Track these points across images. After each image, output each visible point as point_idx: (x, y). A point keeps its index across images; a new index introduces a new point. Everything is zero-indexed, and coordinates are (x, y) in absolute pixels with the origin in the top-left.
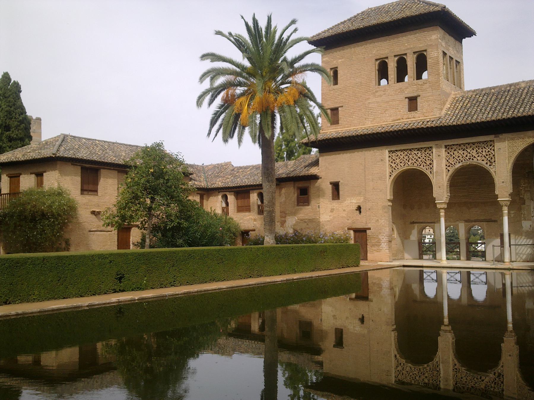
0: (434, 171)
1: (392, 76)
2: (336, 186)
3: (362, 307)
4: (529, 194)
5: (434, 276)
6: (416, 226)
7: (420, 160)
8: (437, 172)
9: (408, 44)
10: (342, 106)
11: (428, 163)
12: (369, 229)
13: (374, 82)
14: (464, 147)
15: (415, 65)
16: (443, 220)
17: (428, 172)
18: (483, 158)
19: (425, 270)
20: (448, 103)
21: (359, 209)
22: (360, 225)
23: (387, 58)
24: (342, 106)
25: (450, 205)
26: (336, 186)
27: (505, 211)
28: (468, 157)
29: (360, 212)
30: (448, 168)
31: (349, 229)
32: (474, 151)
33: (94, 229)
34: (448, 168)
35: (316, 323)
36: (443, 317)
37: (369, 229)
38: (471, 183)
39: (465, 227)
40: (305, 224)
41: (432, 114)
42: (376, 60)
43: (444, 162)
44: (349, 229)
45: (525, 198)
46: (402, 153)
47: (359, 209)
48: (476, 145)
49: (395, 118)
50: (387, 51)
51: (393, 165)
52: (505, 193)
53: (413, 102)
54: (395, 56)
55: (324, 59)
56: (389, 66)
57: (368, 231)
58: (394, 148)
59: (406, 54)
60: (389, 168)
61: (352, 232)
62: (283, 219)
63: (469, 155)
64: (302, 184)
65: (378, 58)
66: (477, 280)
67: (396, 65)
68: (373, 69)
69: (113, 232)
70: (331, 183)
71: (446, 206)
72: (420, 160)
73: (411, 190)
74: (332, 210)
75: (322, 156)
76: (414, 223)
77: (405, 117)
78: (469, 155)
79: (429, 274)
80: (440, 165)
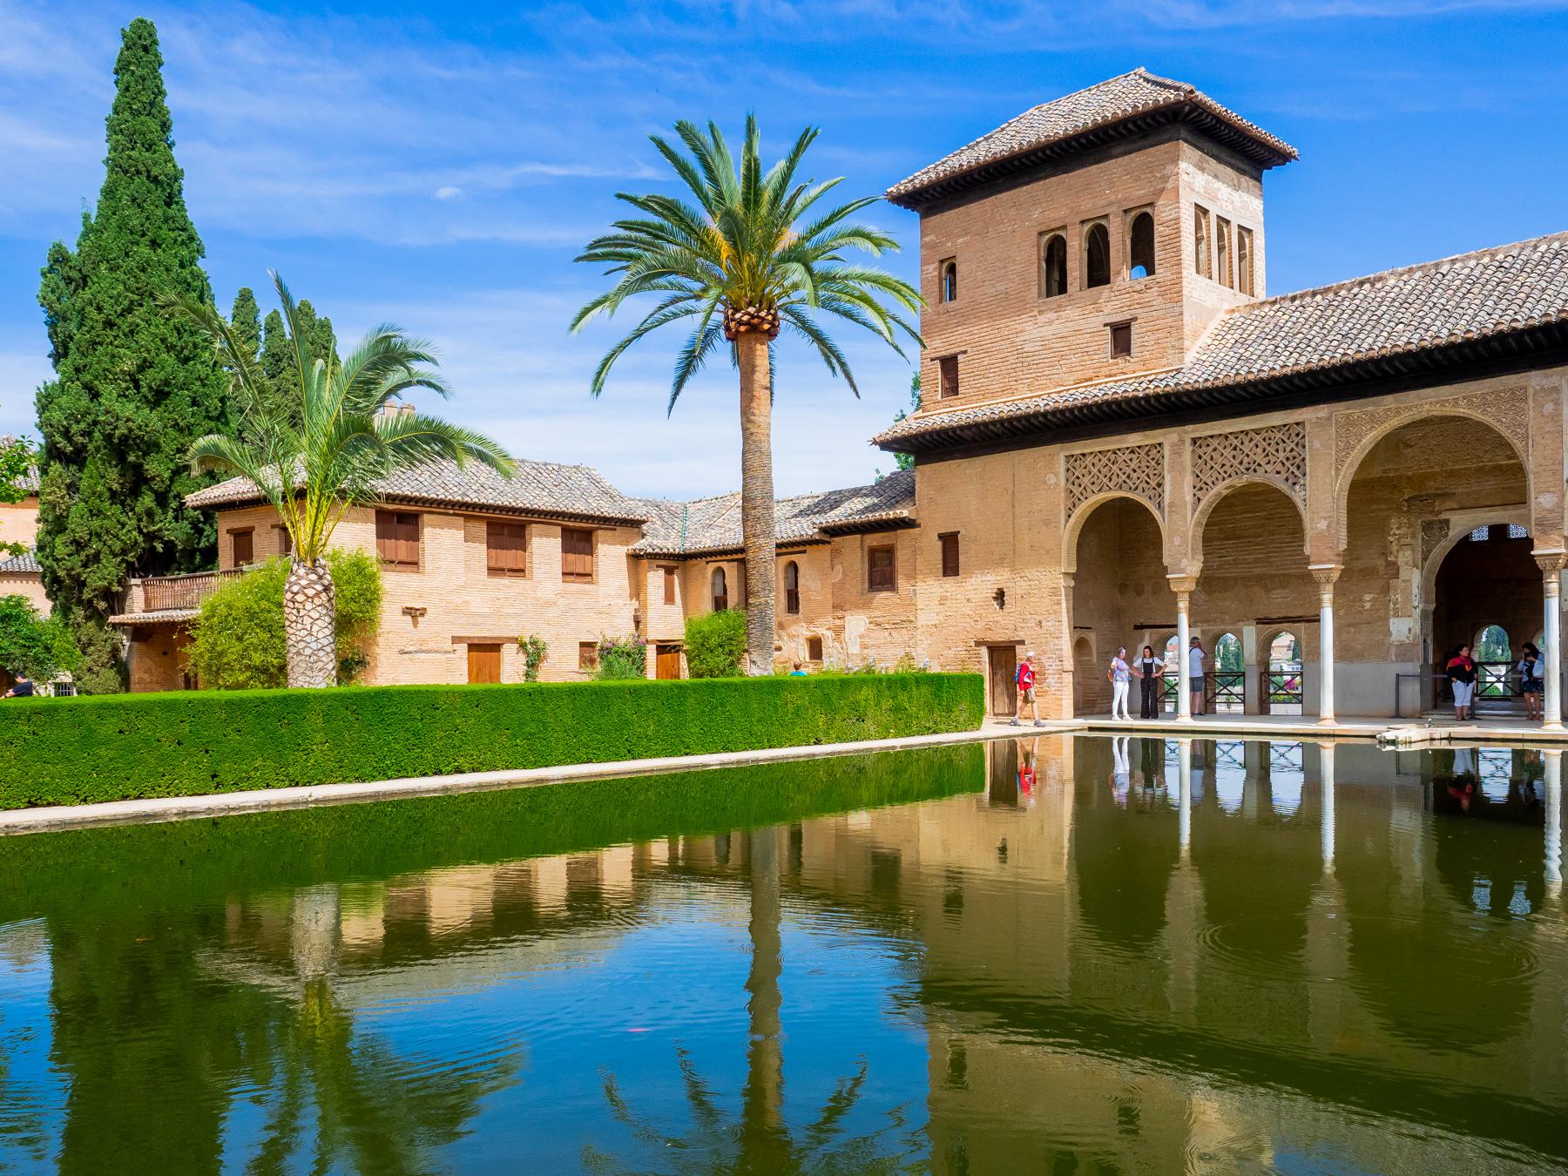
0: (1167, 500)
1: (1077, 274)
2: (950, 542)
3: (1005, 824)
4: (1409, 553)
5: (1296, 756)
6: (1147, 633)
7: (1134, 476)
8: (1171, 505)
9: (1105, 189)
10: (965, 352)
11: (1153, 484)
12: (1022, 642)
13: (1035, 290)
14: (1235, 442)
15: (1128, 242)
16: (1184, 620)
17: (1151, 506)
18: (1279, 467)
19: (1273, 741)
20: (1207, 333)
21: (1000, 596)
22: (999, 636)
23: (1064, 227)
24: (965, 352)
25: (1207, 582)
26: (950, 542)
27: (1327, 597)
28: (1245, 465)
29: (1002, 605)
30: (1199, 494)
31: (978, 644)
32: (1259, 450)
33: (411, 649)
34: (1199, 494)
35: (906, 859)
36: (1321, 861)
37: (1022, 642)
38: (1252, 526)
39: (1258, 633)
40: (886, 633)
41: (1164, 361)
42: (1041, 234)
43: (1189, 480)
44: (978, 644)
45: (1401, 561)
46: (1096, 461)
47: (1000, 596)
48: (1264, 434)
49: (1079, 375)
50: (1064, 212)
51: (1077, 490)
52: (1326, 552)
53: (1121, 336)
54: (1082, 222)
55: (927, 239)
56: (1069, 250)
57: (1019, 649)
58: (1077, 448)
59: (1106, 216)
60: (1067, 499)
61: (984, 651)
62: (838, 622)
63: (1246, 460)
64: (875, 540)
65: (1044, 228)
66: (1282, 761)
67: (1085, 245)
68: (1028, 261)
69: (458, 655)
70: (941, 537)
71: (1193, 587)
72: (1134, 476)
73: (1117, 546)
74: (942, 601)
75: (927, 469)
76: (1142, 627)
77: (1105, 371)
78: (1246, 460)
79: (1282, 750)
80: (1180, 488)
